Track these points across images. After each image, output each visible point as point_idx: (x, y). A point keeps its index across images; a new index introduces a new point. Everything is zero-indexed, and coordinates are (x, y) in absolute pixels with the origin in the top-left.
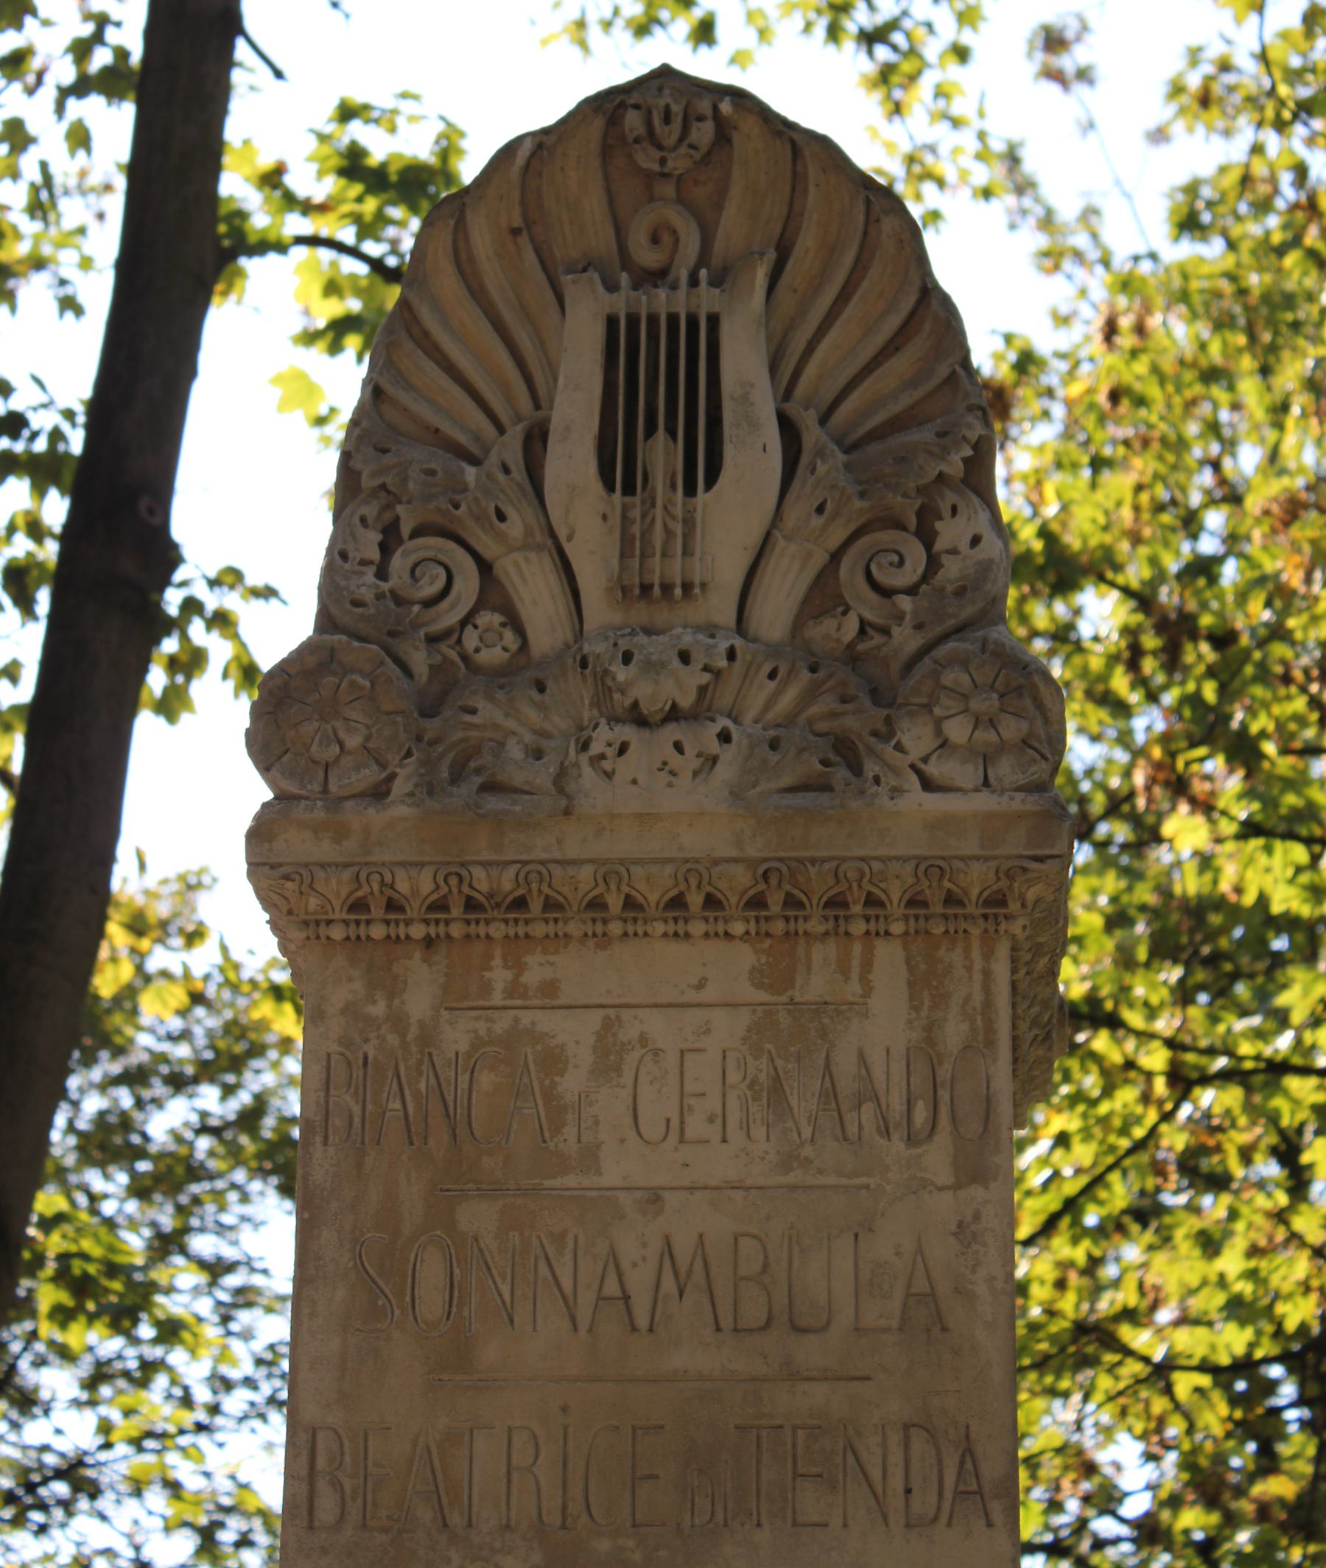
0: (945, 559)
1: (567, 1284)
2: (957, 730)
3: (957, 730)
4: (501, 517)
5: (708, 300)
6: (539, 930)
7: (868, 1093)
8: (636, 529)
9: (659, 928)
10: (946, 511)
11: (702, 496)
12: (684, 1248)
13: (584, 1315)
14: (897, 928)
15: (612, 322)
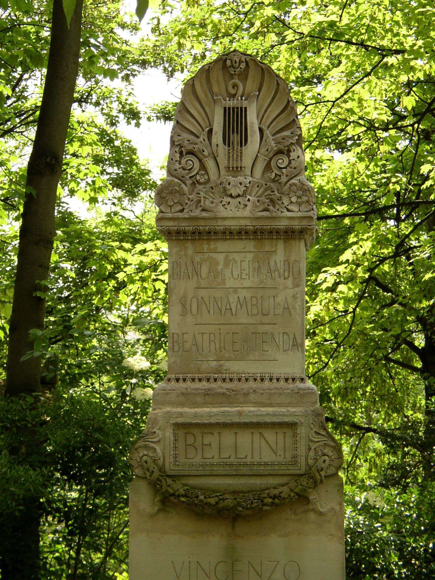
0: (292, 161)
1: (220, 306)
2: (294, 199)
3: (294, 199)
4: (203, 151)
5: (245, 104)
6: (213, 237)
7: (277, 270)
8: (231, 155)
9: (236, 237)
10: (292, 150)
11: (244, 147)
12: (242, 299)
13: (223, 312)
14: (282, 237)
15: (225, 108)
